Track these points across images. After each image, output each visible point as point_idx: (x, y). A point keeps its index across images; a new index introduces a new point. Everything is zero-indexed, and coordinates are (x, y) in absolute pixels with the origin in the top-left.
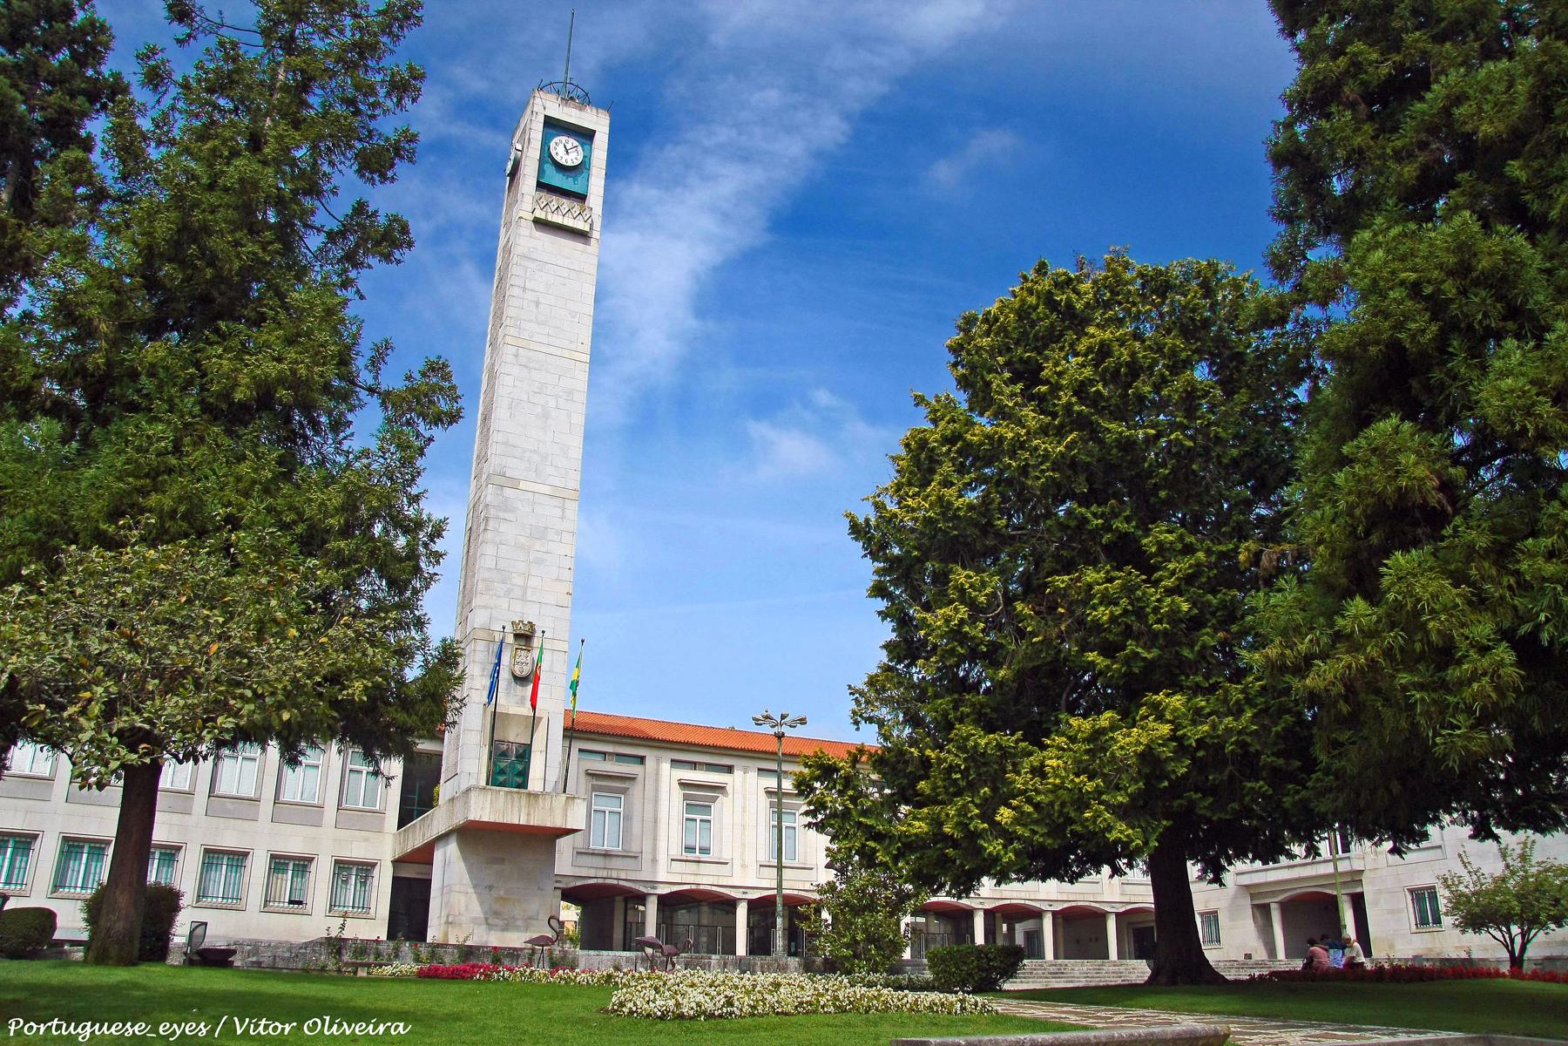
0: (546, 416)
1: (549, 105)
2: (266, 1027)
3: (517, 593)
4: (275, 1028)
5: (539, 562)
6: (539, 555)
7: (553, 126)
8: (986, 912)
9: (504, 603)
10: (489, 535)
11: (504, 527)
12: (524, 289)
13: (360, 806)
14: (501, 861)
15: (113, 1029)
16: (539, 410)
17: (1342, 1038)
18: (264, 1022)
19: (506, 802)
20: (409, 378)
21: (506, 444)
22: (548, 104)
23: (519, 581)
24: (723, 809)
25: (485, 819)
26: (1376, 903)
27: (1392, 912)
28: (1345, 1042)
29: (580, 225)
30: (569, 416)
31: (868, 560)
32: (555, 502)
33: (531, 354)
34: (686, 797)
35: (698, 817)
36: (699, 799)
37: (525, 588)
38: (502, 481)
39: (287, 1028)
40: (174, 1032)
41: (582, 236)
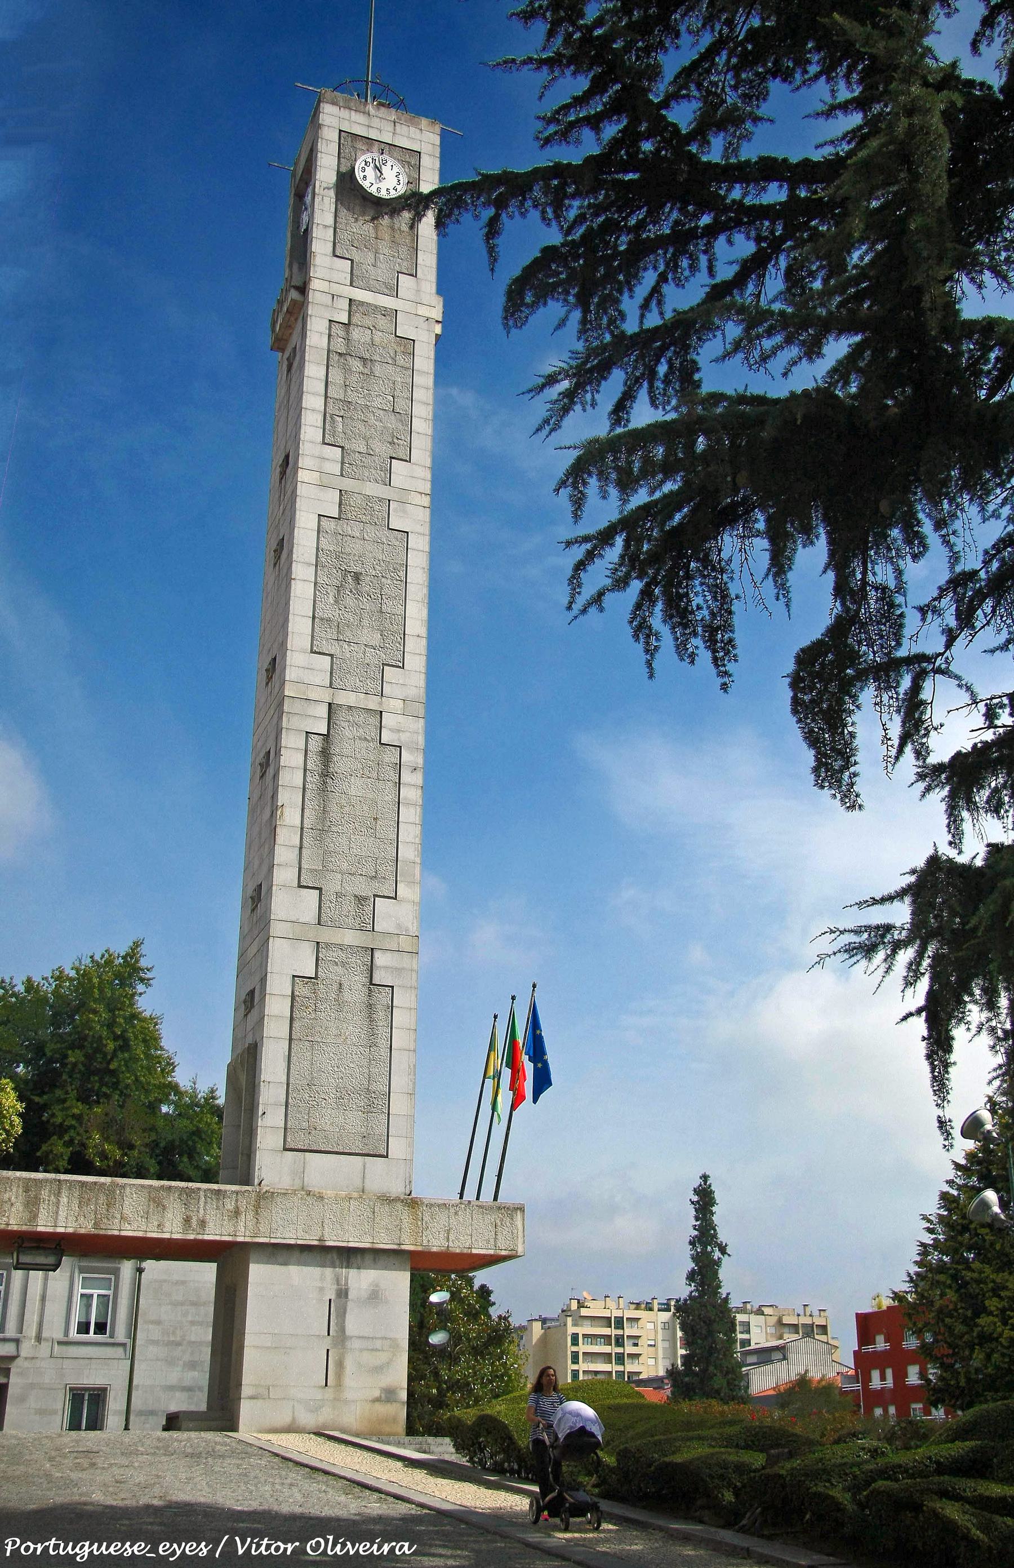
2: (268, 1547)
4: (277, 1549)
13: (110, 1292)
15: (112, 1549)
17: (452, 1557)
18: (265, 1541)
20: (950, 1121)
26: (22, 1399)
27: (41, 1412)
28: (451, 1562)
39: (290, 1547)
40: (174, 1552)
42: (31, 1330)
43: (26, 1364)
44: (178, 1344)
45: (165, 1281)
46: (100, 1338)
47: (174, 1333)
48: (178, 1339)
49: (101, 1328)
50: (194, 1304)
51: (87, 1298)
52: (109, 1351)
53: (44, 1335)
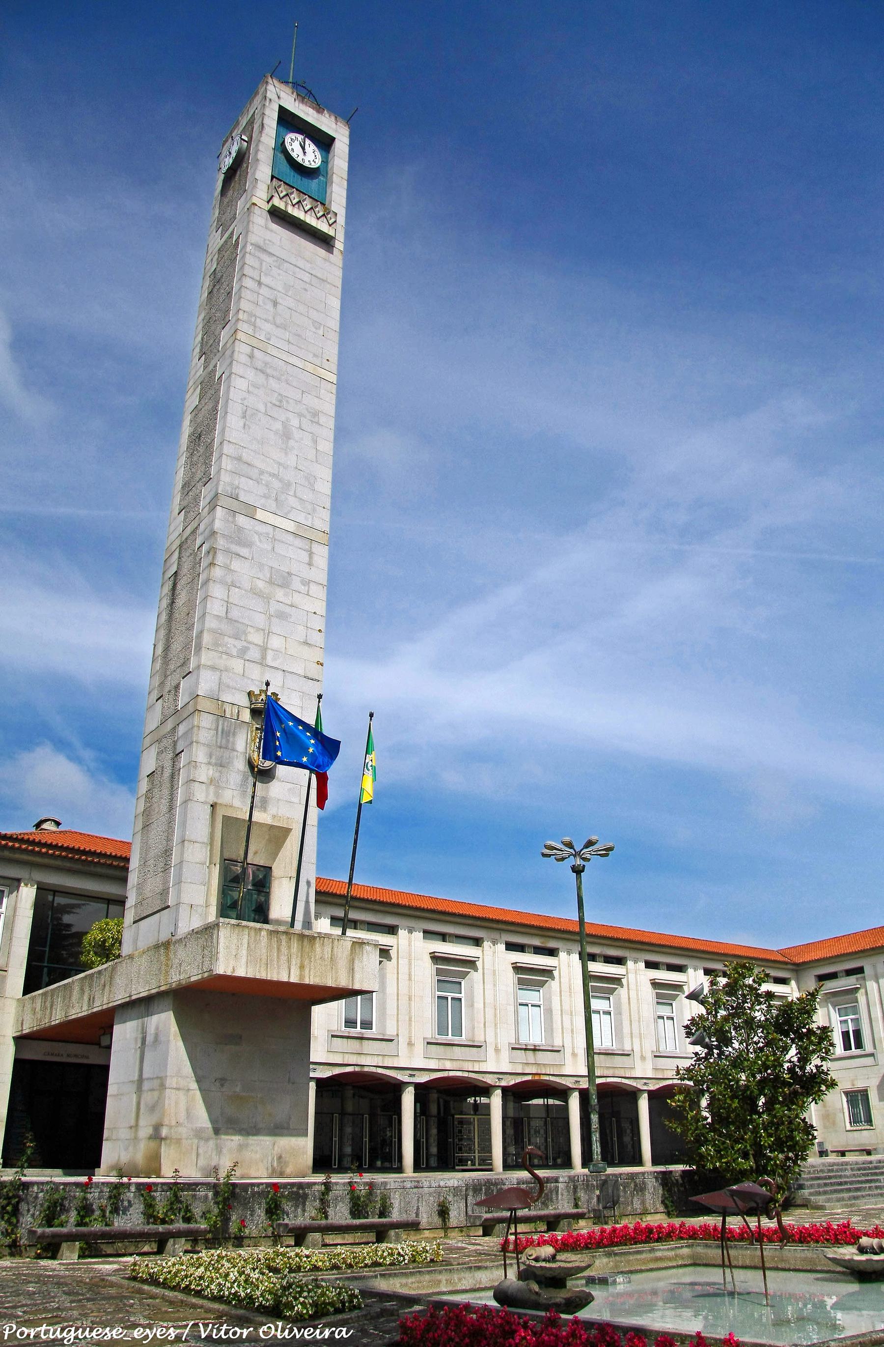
0: (286, 435)
1: (279, 96)
2: (226, 1333)
3: (254, 654)
4: (235, 1333)
5: (282, 616)
6: (282, 607)
7: (288, 121)
8: (505, 1090)
9: (237, 665)
10: (217, 572)
11: (236, 565)
12: (260, 283)
14: (236, 1039)
15: (94, 1334)
16: (278, 426)
18: (225, 1327)
19: (269, 946)
21: (239, 459)
22: (282, 94)
23: (256, 638)
25: (241, 972)
29: (322, 226)
30: (315, 442)
32: (298, 542)
33: (268, 359)
34: (439, 972)
35: (450, 995)
36: (451, 972)
37: (264, 649)
38: (235, 505)
40: (147, 1337)
41: (325, 241)
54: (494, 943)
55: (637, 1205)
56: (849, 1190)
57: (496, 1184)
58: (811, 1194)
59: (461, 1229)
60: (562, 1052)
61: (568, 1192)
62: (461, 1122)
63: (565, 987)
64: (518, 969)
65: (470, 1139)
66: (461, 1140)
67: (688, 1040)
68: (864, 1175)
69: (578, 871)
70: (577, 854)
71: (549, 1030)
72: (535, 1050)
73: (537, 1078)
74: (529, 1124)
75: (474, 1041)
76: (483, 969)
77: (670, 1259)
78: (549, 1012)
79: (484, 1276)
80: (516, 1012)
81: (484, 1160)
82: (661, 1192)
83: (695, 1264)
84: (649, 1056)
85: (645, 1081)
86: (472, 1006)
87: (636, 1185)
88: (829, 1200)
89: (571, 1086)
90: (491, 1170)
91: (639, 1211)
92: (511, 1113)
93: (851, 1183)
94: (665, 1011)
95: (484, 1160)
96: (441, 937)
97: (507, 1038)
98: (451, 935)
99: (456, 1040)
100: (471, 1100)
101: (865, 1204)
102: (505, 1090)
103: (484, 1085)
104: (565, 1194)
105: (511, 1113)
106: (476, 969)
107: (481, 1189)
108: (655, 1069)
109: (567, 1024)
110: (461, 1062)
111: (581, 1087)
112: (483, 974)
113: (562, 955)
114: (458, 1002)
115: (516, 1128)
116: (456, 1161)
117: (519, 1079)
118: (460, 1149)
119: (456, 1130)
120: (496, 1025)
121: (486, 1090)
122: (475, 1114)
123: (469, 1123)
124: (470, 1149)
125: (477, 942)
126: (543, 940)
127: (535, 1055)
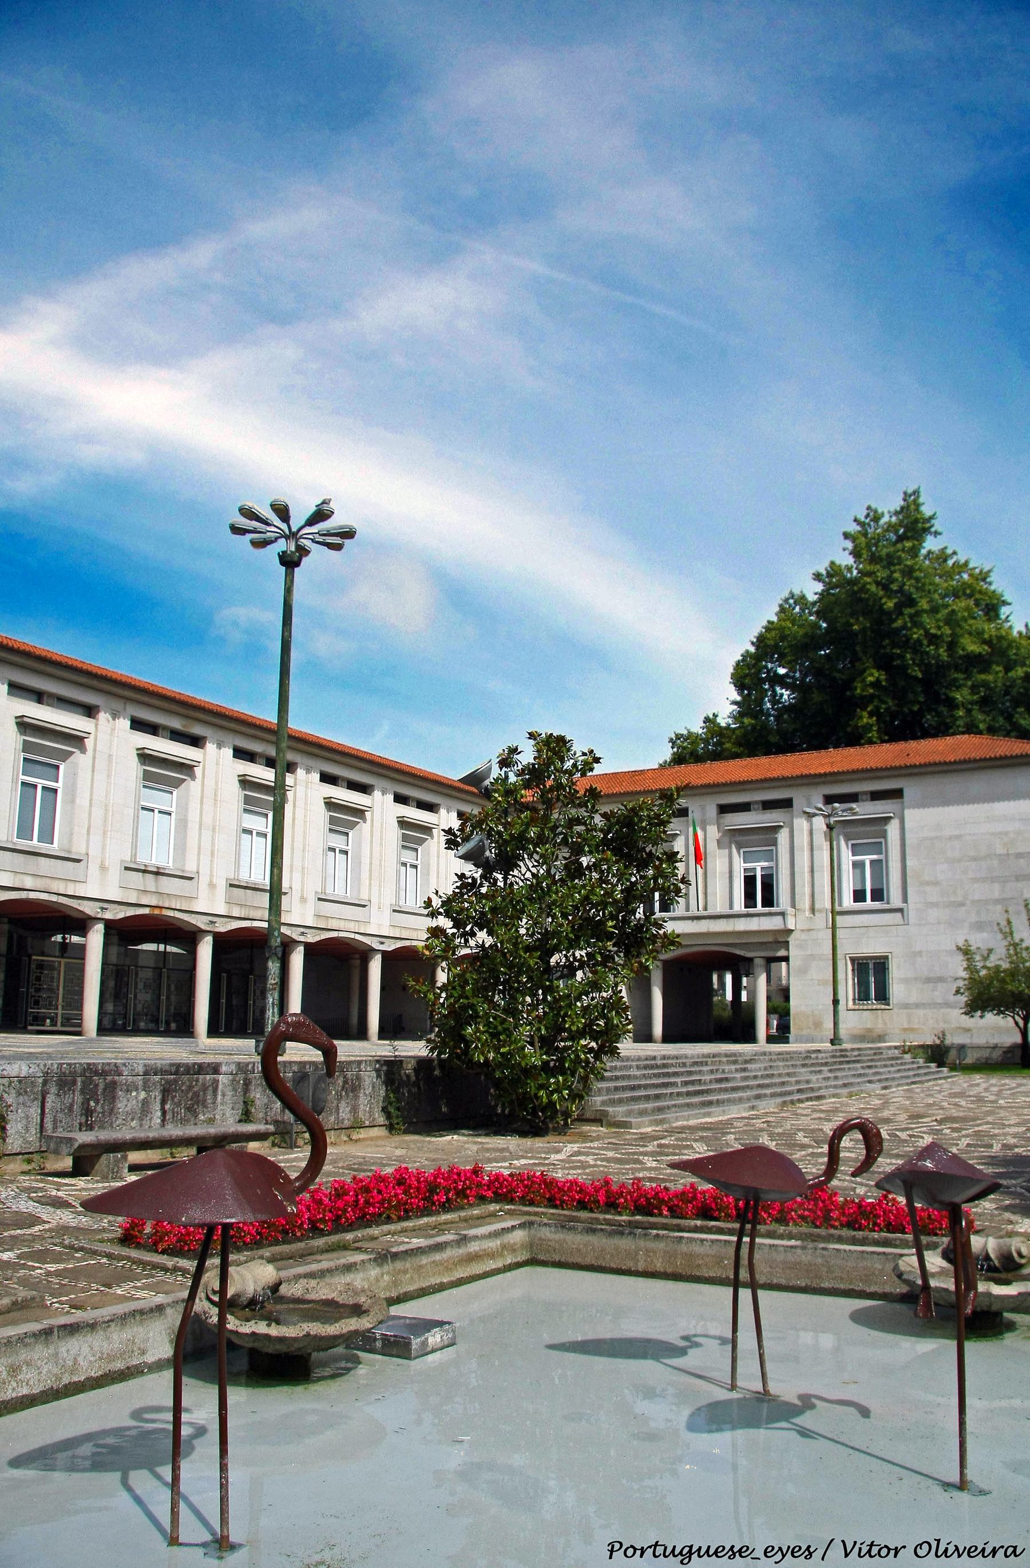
8: (110, 926)
24: (78, 767)
31: (1000, 590)
34: (27, 747)
35: (41, 783)
36: (344, 818)
42: (805, 903)
43: (804, 936)
44: (962, 904)
45: (937, 838)
46: (877, 905)
47: (954, 893)
48: (960, 899)
49: (878, 895)
50: (975, 859)
51: (858, 866)
52: (887, 918)
53: (817, 906)
54: (115, 716)
55: (345, 1112)
56: (647, 1098)
57: (104, 1073)
58: (603, 1103)
59: (27, 1156)
60: (196, 879)
61: (235, 1090)
62: (41, 966)
63: (209, 792)
64: (145, 757)
65: (50, 990)
66: (38, 990)
67: (452, 853)
68: (656, 1076)
69: (289, 563)
70: (292, 536)
71: (181, 848)
72: (157, 873)
73: (157, 912)
74: (137, 974)
75: (69, 852)
76: (95, 750)
77: (492, 1255)
78: (183, 824)
79: (85, 1349)
80: (136, 818)
81: (68, 1019)
82: (382, 1093)
83: (533, 1262)
84: (312, 898)
85: (302, 930)
86: (73, 801)
87: (345, 1082)
88: (629, 1113)
89: (203, 927)
90: (79, 1034)
91: (347, 1123)
92: (113, 959)
93: (646, 1087)
94: (337, 842)
95: (68, 1019)
96: (35, 697)
97: (119, 853)
98: (51, 695)
99: (44, 847)
100: (59, 938)
101: (677, 1119)
102: (110, 926)
103: (80, 916)
104: (230, 1094)
105: (113, 959)
106: (83, 750)
107: (74, 1083)
108: (318, 916)
109: (206, 844)
110: (48, 881)
111: (217, 930)
112: (94, 758)
113: (210, 747)
114: (52, 794)
115: (116, 978)
116: (30, 1018)
117: (131, 912)
118: (37, 1003)
119: (33, 977)
120: (105, 833)
121: (81, 924)
122: (62, 957)
123: (52, 968)
124: (50, 1004)
125: (90, 711)
126: (184, 722)
127: (156, 881)
